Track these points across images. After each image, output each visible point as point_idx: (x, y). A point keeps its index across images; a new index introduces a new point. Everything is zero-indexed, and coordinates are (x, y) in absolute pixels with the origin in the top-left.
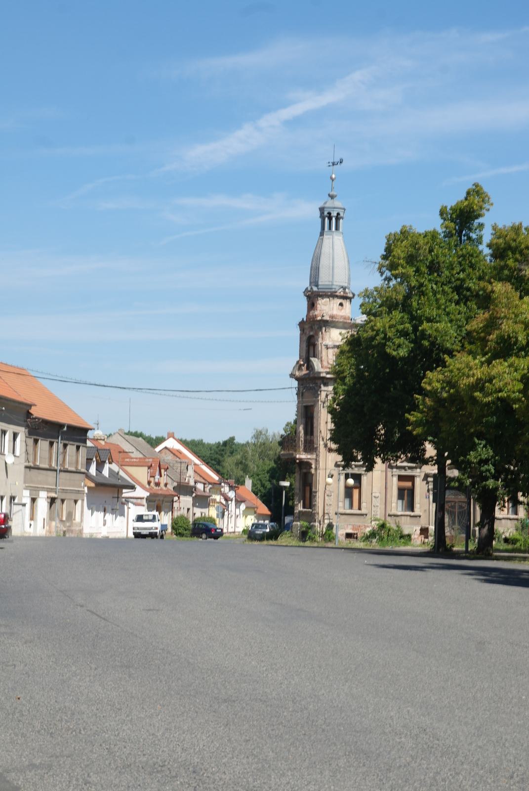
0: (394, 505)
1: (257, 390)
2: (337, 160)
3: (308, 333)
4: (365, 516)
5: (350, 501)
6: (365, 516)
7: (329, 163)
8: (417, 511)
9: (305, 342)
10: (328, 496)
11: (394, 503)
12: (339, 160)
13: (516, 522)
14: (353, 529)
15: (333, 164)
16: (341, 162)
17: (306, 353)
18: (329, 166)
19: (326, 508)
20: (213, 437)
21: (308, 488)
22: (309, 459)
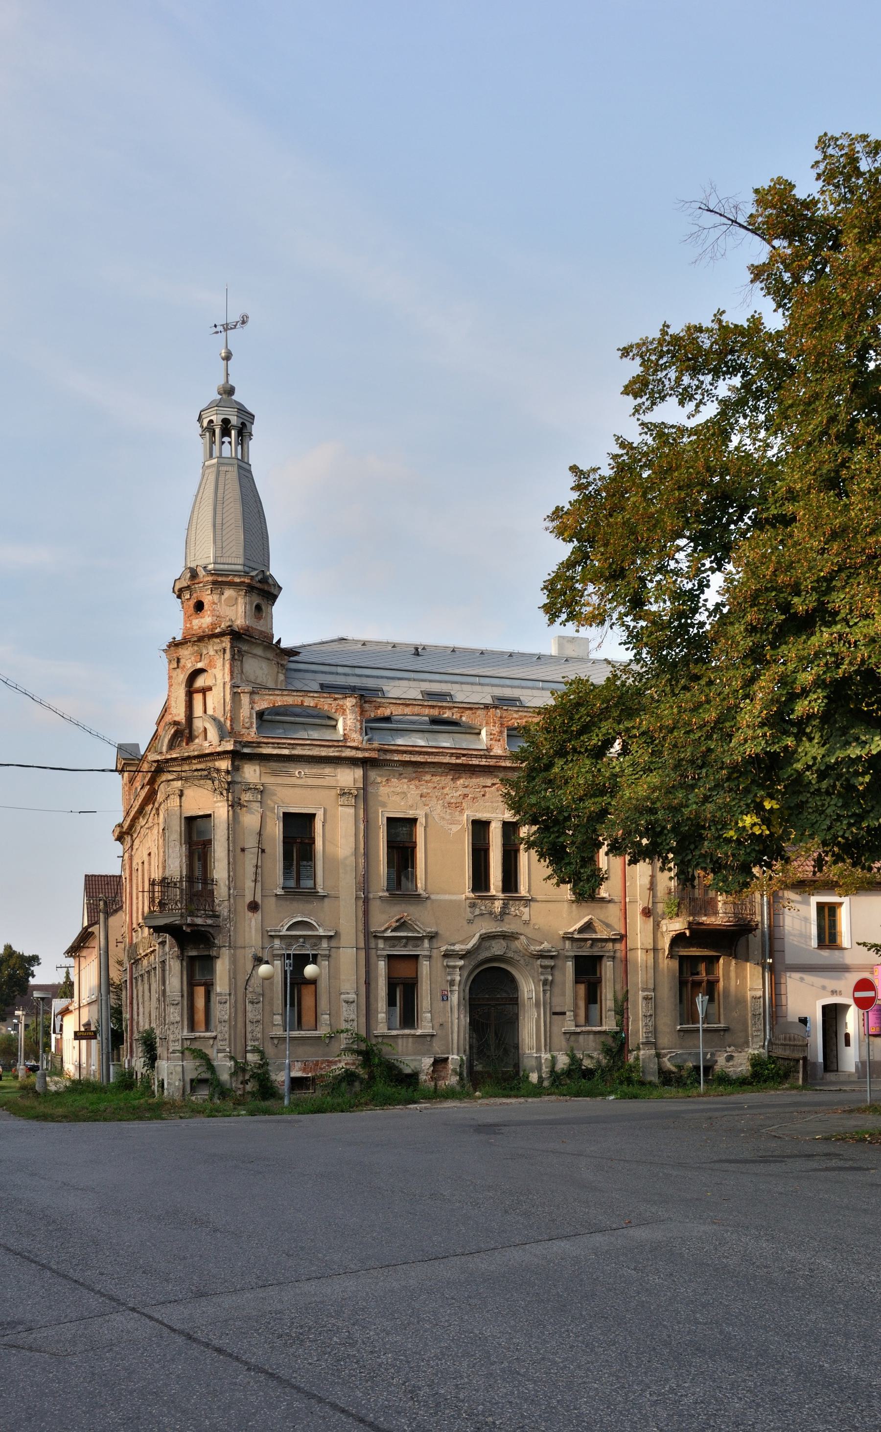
0: (382, 1016)
1: (103, 770)
2: (234, 317)
3: (189, 665)
4: (428, 1039)
5: (796, 975)
6: (428, 1039)
7: (215, 326)
8: (424, 1027)
9: (184, 685)
10: (252, 1003)
11: (381, 1013)
12: (238, 318)
13: (603, 1038)
14: (304, 1070)
15: (226, 328)
16: (244, 322)
17: (186, 707)
18: (217, 332)
19: (249, 1029)
20: (549, 513)
21: (200, 991)
22: (210, 926)
